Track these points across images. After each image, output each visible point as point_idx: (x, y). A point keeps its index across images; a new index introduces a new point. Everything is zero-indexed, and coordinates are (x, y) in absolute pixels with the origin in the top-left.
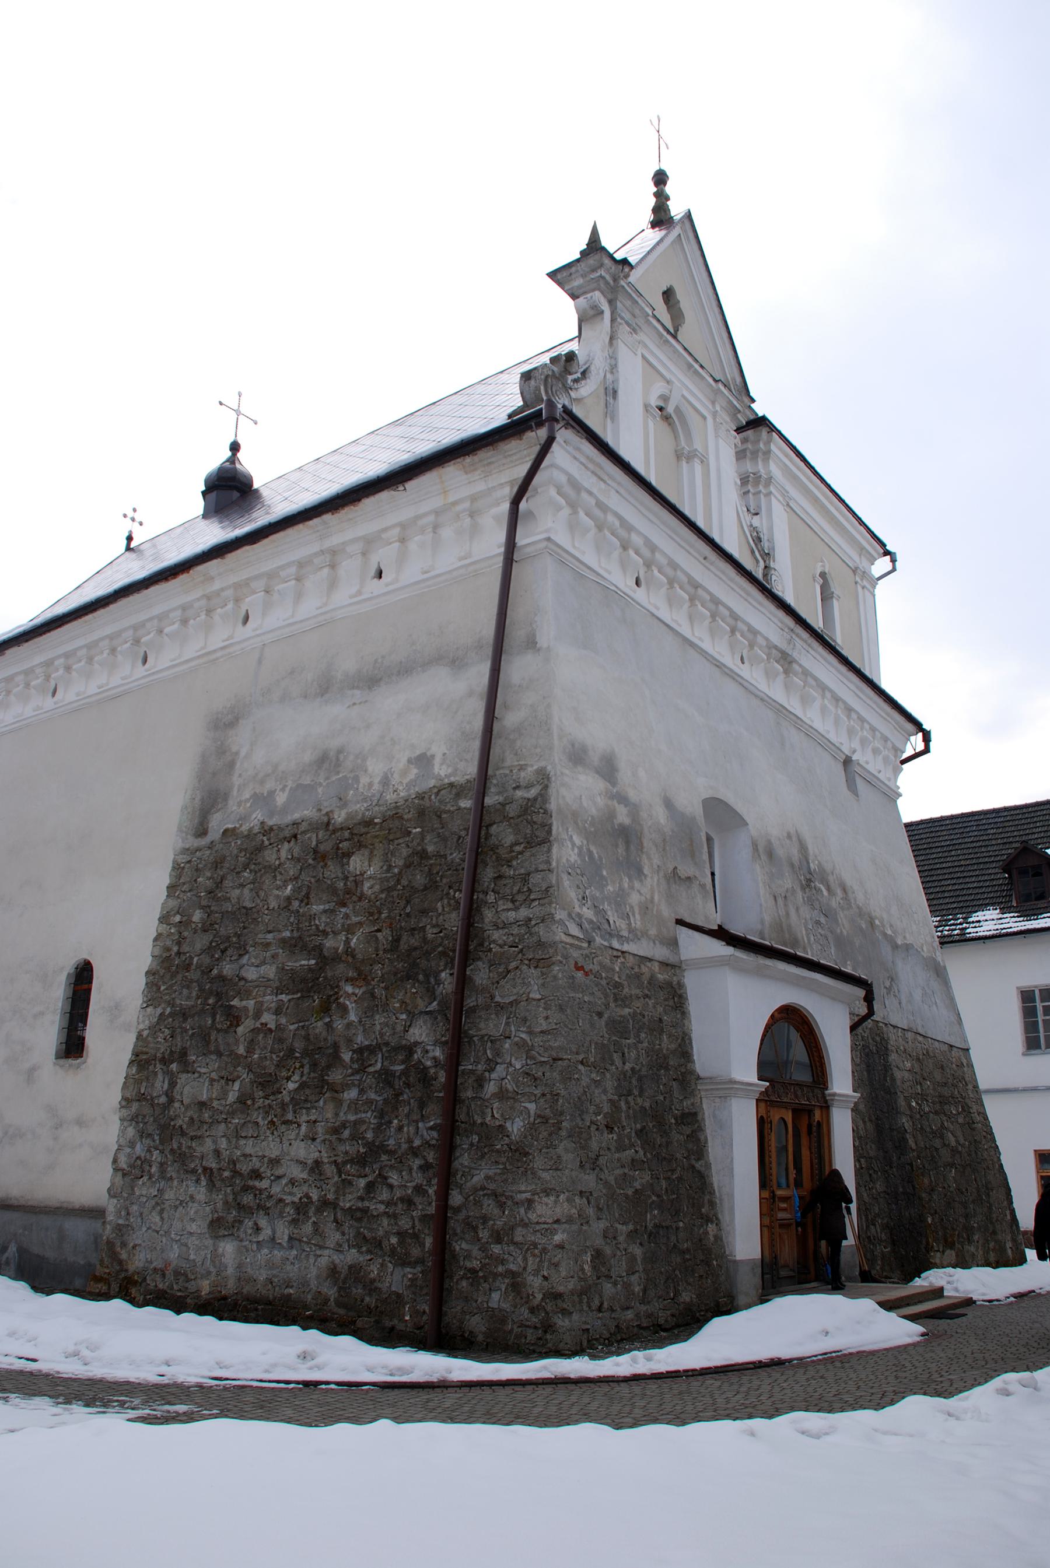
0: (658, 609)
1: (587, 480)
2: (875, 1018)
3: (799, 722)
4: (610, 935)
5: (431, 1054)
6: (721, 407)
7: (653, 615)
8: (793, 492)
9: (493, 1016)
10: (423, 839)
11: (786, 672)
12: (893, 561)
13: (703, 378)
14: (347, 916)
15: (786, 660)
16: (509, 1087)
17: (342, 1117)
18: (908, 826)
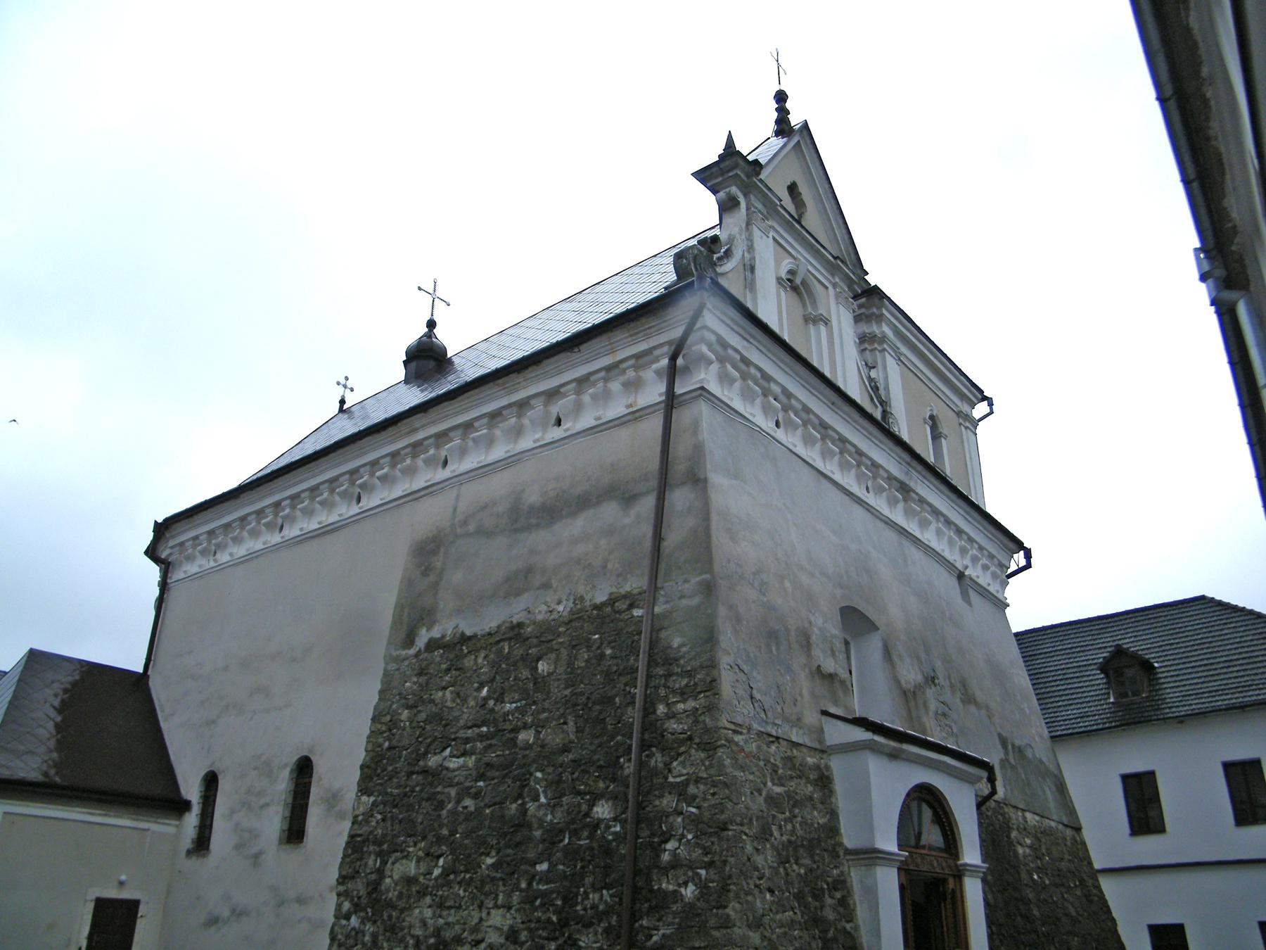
2: (996, 797)
4: (766, 723)
8: (903, 349)
11: (905, 500)
12: (991, 404)
15: (905, 489)
18: (1017, 635)
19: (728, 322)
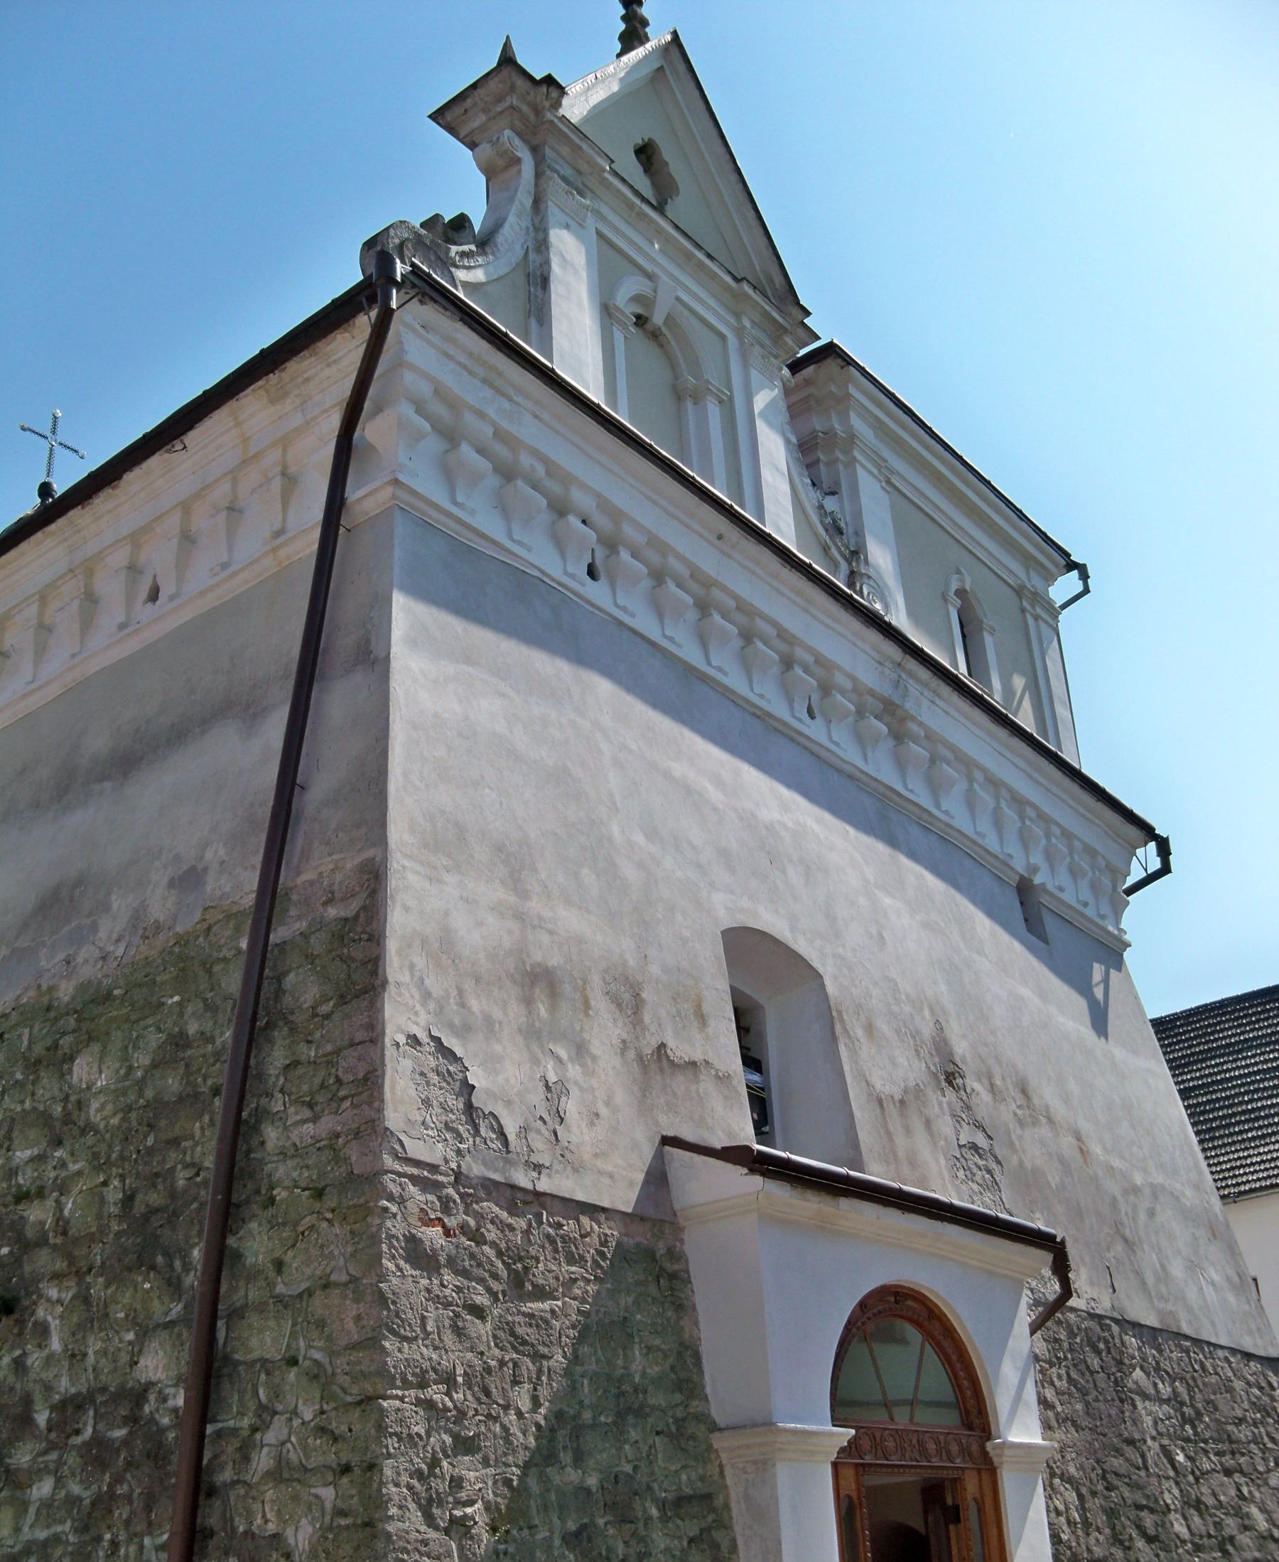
1: (471, 392)
3: (926, 817)
5: (171, 1403)
6: (753, 322)
7: (621, 624)
10: (181, 1014)
12: (1084, 576)
13: (714, 276)
14: (63, 1164)
16: (292, 1456)
17: (26, 1534)
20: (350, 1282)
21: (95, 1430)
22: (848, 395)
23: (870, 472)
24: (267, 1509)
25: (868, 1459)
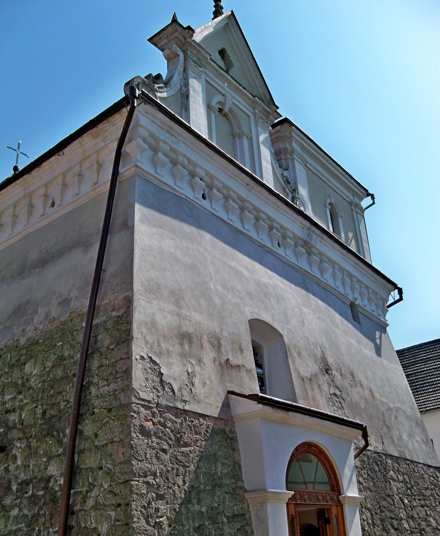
0: (218, 212)
1: (162, 135)
3: (318, 281)
5: (59, 483)
6: (259, 111)
7: (213, 214)
9: (93, 455)
10: (62, 349)
12: (373, 198)
14: (21, 400)
16: (101, 501)
17: (9, 528)
19: (352, 263)
20: (120, 441)
21: (33, 492)
22: (292, 136)
23: (299, 162)
24: (92, 519)
25: (299, 502)
